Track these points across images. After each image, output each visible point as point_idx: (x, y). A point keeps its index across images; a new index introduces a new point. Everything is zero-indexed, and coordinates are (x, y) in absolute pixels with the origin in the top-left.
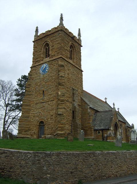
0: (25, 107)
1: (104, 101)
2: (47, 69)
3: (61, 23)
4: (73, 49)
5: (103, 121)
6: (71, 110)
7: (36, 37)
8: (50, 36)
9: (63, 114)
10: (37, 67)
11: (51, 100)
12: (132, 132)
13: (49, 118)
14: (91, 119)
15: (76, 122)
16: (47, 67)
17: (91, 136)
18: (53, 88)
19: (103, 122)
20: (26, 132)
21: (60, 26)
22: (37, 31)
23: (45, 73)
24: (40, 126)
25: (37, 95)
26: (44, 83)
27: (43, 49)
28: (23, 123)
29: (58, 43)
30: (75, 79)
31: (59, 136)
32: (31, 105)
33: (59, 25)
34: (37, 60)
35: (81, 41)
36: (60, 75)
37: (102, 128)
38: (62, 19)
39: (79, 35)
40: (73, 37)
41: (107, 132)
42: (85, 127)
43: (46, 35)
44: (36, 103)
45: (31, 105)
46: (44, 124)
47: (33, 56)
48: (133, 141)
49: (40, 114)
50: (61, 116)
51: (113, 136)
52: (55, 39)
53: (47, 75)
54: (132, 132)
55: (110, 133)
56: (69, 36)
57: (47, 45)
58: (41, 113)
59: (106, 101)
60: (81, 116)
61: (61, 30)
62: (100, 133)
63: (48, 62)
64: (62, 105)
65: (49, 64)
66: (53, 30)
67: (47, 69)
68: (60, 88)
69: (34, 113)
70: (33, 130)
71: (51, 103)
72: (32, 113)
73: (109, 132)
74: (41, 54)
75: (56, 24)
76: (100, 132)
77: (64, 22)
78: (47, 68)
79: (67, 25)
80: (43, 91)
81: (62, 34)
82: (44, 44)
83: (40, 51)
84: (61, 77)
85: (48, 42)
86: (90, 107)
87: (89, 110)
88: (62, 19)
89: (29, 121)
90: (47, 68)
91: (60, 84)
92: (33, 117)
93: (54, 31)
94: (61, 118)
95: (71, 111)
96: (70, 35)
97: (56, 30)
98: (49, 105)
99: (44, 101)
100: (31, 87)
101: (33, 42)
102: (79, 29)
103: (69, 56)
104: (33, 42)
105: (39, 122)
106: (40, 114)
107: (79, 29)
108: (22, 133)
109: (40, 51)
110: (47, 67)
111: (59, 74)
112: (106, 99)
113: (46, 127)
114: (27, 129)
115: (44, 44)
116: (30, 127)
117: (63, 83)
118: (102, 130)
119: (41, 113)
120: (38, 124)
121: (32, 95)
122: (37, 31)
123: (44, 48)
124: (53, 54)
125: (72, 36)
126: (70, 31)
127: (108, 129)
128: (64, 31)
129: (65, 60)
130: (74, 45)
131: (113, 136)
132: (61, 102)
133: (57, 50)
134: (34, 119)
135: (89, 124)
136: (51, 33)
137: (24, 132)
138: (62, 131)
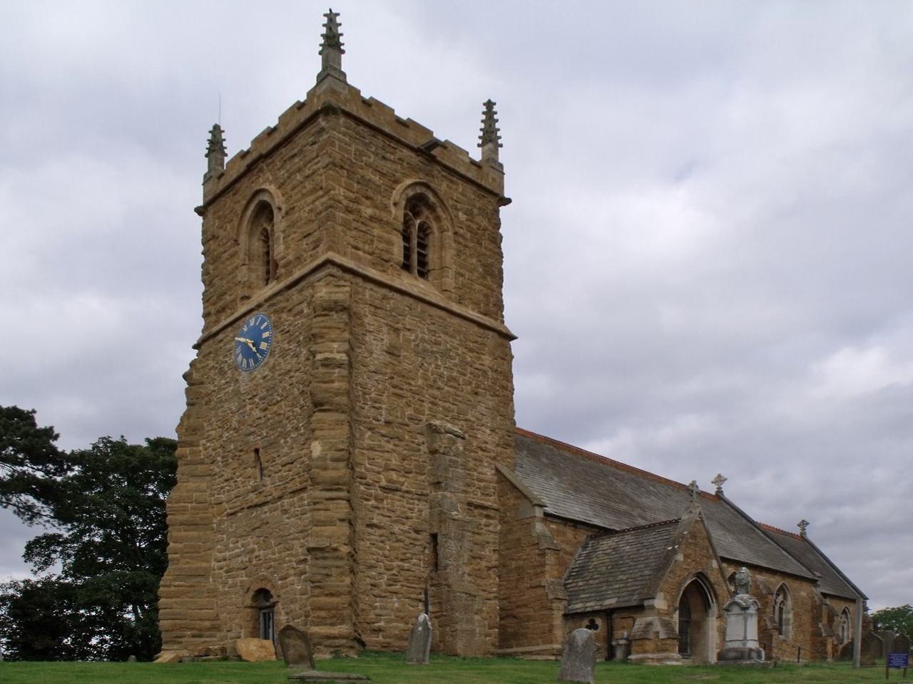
0: (183, 534)
1: (712, 490)
2: (266, 340)
3: (331, 71)
4: (438, 219)
5: (623, 573)
6: (417, 532)
7: (210, 185)
8: (277, 160)
9: (335, 550)
10: (221, 336)
11: (292, 486)
12: (736, 610)
13: (292, 572)
14: (547, 568)
15: (449, 586)
16: (266, 329)
17: (544, 643)
18: (297, 429)
19: (621, 577)
20: (200, 636)
21: (318, 92)
22: (216, 145)
23: (256, 361)
24: (261, 609)
25: (230, 475)
26: (257, 413)
27: (243, 239)
28: (178, 600)
29: (313, 191)
30: (451, 379)
31: (319, 644)
32: (212, 523)
33: (364, 101)
34: (221, 304)
35: (499, 169)
36: (319, 357)
37: (611, 602)
38: (332, 43)
39: (490, 136)
40: (430, 151)
41: (634, 620)
42: (518, 607)
43: (254, 155)
44: (232, 511)
45: (212, 523)
46: (272, 600)
47: (202, 288)
48: (735, 650)
49: (250, 561)
50: (325, 558)
51: (662, 636)
52: (299, 170)
53: (266, 373)
54: (736, 610)
55: (650, 624)
56: (399, 142)
57: (265, 210)
58: (257, 553)
59: (719, 492)
60: (495, 556)
61: (328, 110)
62: (596, 627)
63: (266, 301)
64: (331, 505)
65: (276, 312)
66: (287, 124)
67: (266, 340)
68: (319, 421)
69: (227, 554)
70: (231, 627)
71: (292, 505)
72: (220, 555)
73: (641, 621)
74: (237, 268)
75: (296, 81)
76: (599, 621)
77: (346, 64)
78: (266, 335)
79: (366, 74)
80: (257, 451)
81: (337, 130)
82: (249, 212)
83: (232, 256)
84: (326, 366)
85: (265, 197)
86: (547, 515)
87: (539, 527)
88: (332, 43)
89: (213, 593)
90: (266, 335)
91: (318, 405)
92: (227, 572)
93: (293, 125)
94: (325, 568)
95: (424, 538)
96: (410, 138)
97: (305, 114)
98: (285, 512)
99: (262, 499)
100: (204, 441)
101: (200, 211)
102: (489, 105)
103: (398, 253)
104: (200, 211)
105: (251, 593)
106: (250, 561)
107: (489, 105)
108: (183, 640)
109: (232, 256)
110: (266, 329)
111: (314, 354)
112: (720, 480)
113: (283, 612)
114: (207, 624)
115: (249, 212)
116: (217, 618)
117: (337, 395)
118: (608, 613)
119: (257, 553)
120: (249, 602)
121: (209, 475)
122: (216, 145)
123: (251, 234)
124: (291, 257)
125: (422, 142)
126: (366, 94)
127: (640, 608)
128: (348, 115)
129: (366, 279)
130: (436, 194)
131: (662, 636)
132: (328, 490)
133: (306, 229)
134: (230, 581)
135: (540, 591)
136: (277, 138)
137: (194, 636)
138: (332, 625)
